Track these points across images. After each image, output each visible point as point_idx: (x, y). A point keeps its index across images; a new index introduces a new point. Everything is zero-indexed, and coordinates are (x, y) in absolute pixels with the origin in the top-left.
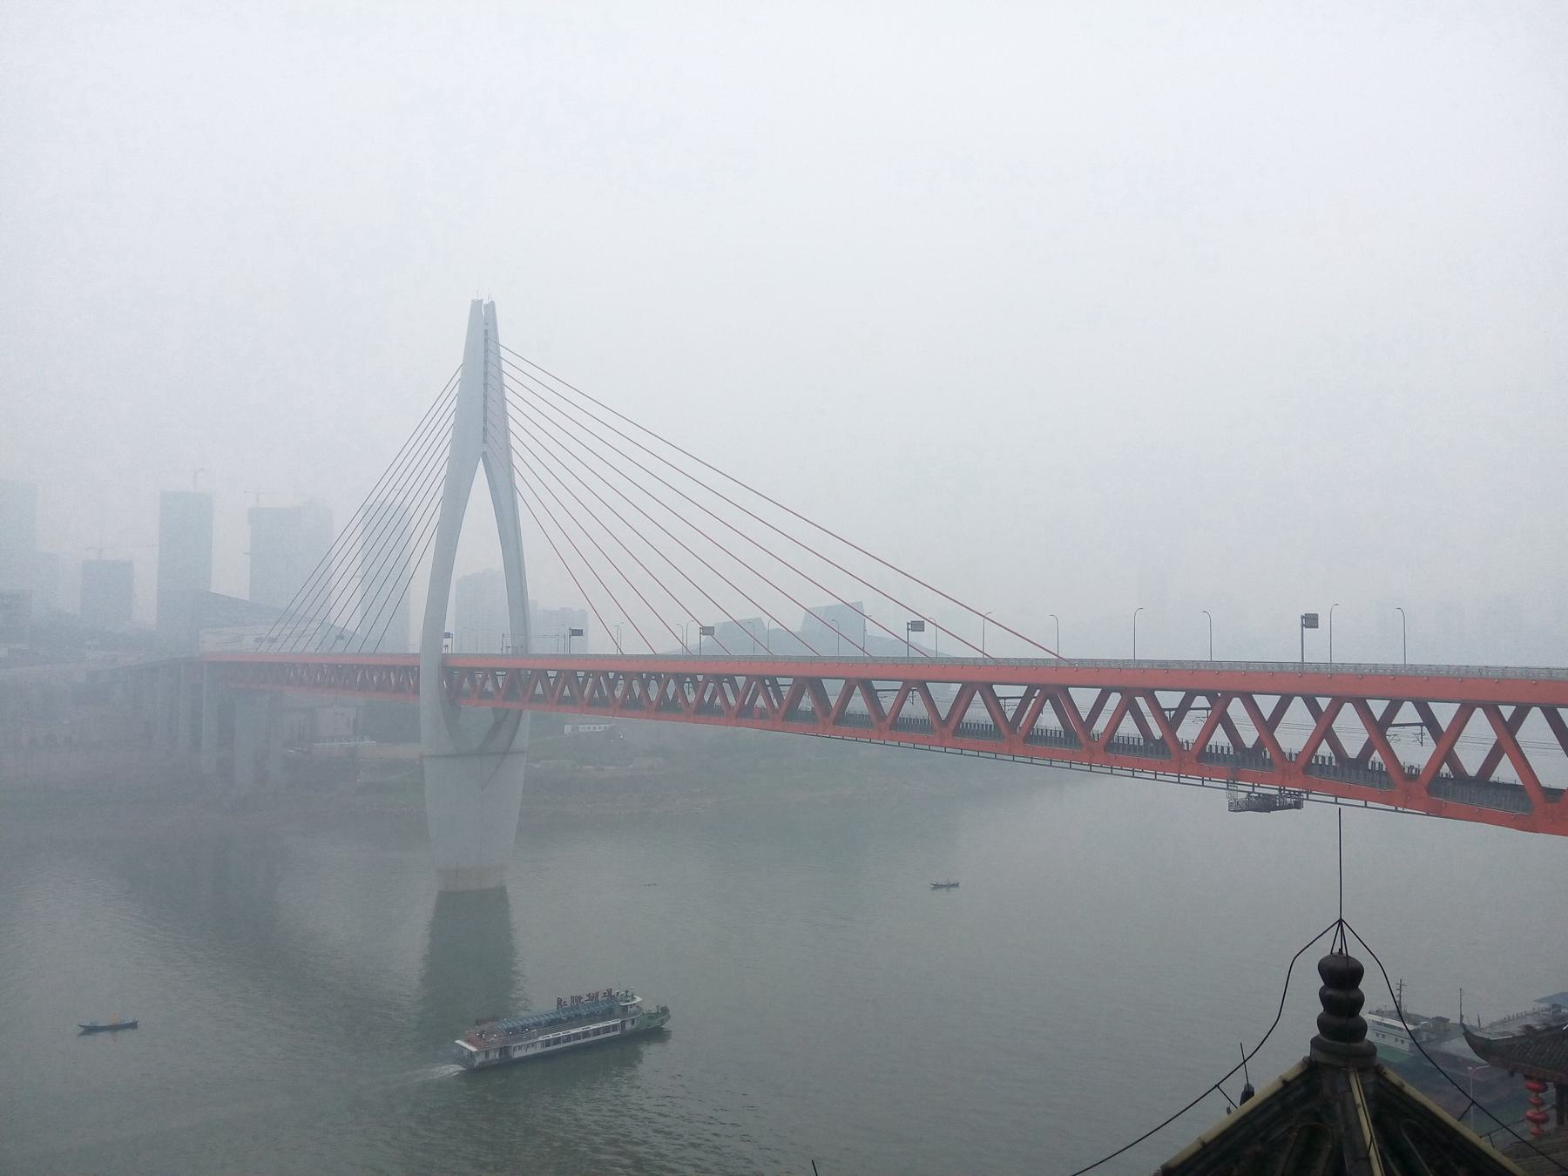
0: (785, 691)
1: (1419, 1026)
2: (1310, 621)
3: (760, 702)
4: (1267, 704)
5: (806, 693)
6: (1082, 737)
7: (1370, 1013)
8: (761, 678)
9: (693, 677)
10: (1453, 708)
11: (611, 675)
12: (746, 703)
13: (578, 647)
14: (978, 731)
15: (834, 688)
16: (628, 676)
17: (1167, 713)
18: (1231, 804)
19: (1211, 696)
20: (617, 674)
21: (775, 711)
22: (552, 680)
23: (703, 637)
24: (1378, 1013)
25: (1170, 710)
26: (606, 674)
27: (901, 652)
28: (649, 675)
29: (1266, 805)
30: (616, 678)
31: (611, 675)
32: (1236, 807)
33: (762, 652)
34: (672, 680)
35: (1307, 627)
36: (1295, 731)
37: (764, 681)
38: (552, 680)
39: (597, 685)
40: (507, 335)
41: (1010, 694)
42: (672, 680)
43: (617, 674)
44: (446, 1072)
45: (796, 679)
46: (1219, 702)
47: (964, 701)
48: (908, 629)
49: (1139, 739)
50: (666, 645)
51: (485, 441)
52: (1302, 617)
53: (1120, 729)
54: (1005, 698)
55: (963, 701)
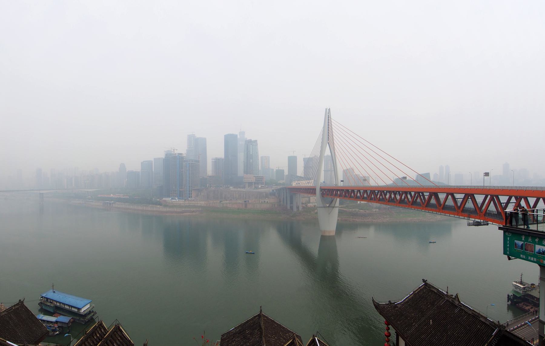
0: (426, 197)
1: (525, 287)
2: (487, 174)
3: (419, 200)
4: (532, 201)
5: (433, 197)
6: (478, 212)
7: (514, 282)
8: (419, 193)
9: (399, 192)
10: (535, 199)
11: (385, 192)
12: (414, 200)
13: (366, 184)
14: (433, 206)
15: (442, 196)
16: (390, 192)
17: (502, 204)
18: (468, 224)
19: (516, 198)
20: (378, 191)
21: (423, 203)
22: (376, 193)
23: (485, 177)
24: (516, 282)
25: (503, 203)
26: (383, 191)
27: (481, 184)
28: (397, 192)
29: (478, 224)
30: (386, 193)
31: (385, 192)
32: (469, 225)
33: (377, 185)
34: (392, 193)
35: (485, 176)
36: (398, 197)
37: (419, 193)
38: (376, 193)
39: (381, 195)
40: (333, 116)
41: (459, 197)
42: (392, 193)
43: (378, 191)
44: (279, 188)
45: (364, 190)
46: (518, 199)
47: (465, 201)
48: (484, 176)
49: (495, 212)
50: (381, 184)
51: (328, 140)
52: (484, 173)
53: (466, 206)
54: (457, 199)
55: (465, 200)
